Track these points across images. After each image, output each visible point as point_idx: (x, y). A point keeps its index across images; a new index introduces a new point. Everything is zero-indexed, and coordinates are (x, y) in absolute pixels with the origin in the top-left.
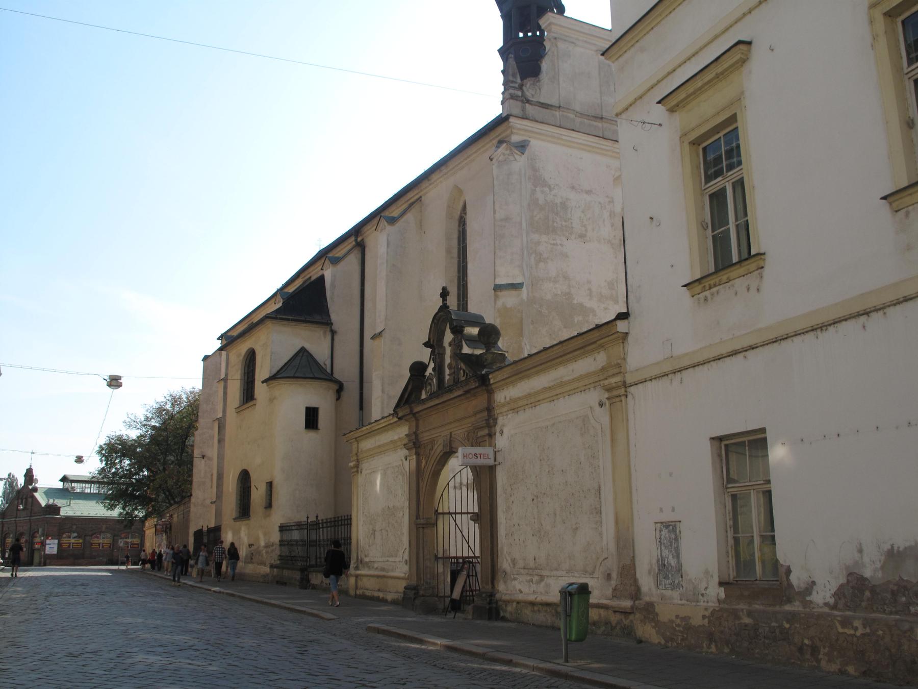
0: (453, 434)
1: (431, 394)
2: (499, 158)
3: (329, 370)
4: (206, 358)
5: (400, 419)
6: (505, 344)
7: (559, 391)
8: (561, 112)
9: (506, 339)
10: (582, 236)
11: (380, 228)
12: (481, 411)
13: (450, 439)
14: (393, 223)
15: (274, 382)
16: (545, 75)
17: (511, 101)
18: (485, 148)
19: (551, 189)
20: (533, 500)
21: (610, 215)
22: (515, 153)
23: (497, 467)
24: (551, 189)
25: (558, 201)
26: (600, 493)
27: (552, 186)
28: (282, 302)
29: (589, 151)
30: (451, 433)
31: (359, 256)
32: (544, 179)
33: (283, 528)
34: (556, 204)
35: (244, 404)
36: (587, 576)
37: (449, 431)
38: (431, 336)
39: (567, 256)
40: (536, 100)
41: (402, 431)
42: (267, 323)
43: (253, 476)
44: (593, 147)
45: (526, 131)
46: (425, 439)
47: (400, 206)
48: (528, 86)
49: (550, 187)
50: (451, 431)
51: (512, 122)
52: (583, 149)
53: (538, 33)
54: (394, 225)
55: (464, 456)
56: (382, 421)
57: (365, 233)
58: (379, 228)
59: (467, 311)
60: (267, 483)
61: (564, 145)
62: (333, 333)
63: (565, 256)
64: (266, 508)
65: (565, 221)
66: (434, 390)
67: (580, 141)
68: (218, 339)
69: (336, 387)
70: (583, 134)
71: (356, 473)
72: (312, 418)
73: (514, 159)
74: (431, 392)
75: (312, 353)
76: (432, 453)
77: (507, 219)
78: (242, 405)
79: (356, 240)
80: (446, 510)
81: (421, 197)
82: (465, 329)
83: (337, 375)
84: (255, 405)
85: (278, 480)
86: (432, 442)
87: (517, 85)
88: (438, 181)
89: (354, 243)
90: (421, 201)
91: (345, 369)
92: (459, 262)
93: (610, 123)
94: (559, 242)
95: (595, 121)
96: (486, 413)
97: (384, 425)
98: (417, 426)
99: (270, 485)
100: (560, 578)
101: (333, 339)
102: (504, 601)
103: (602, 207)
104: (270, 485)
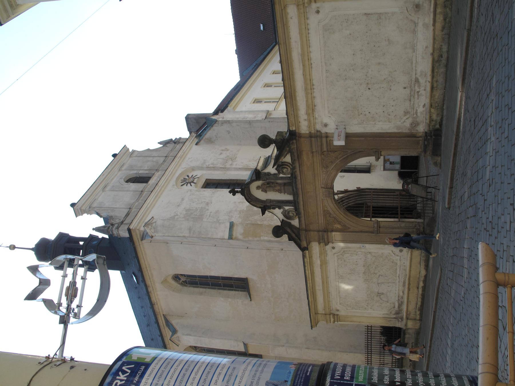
0: (323, 186)
2: (152, 232)
6: (265, 235)
7: (306, 58)
8: (133, 208)
9: (262, 234)
10: (207, 204)
11: (177, 342)
13: (325, 188)
14: (176, 331)
16: (109, 214)
17: (120, 229)
18: (144, 254)
21: (198, 191)
23: (348, 132)
25: (184, 212)
26: (369, 14)
27: (175, 214)
32: (170, 217)
34: (186, 213)
36: (416, 30)
39: (218, 211)
41: (315, 247)
44: (157, 195)
45: (139, 223)
47: (166, 334)
48: (113, 221)
50: (320, 187)
51: (133, 228)
53: (81, 243)
55: (339, 140)
58: (177, 342)
61: (152, 208)
63: (217, 212)
65: (197, 210)
66: (293, 209)
67: (152, 200)
70: (149, 198)
71: (338, 316)
73: (155, 223)
74: (294, 211)
77: (190, 229)
82: (258, 169)
86: (326, 213)
87: (111, 227)
88: (157, 298)
92: (209, 288)
93: (146, 188)
94: (209, 214)
95: (143, 195)
96: (313, 139)
97: (310, 272)
100: (417, 61)
102: (430, 122)
103: (192, 195)
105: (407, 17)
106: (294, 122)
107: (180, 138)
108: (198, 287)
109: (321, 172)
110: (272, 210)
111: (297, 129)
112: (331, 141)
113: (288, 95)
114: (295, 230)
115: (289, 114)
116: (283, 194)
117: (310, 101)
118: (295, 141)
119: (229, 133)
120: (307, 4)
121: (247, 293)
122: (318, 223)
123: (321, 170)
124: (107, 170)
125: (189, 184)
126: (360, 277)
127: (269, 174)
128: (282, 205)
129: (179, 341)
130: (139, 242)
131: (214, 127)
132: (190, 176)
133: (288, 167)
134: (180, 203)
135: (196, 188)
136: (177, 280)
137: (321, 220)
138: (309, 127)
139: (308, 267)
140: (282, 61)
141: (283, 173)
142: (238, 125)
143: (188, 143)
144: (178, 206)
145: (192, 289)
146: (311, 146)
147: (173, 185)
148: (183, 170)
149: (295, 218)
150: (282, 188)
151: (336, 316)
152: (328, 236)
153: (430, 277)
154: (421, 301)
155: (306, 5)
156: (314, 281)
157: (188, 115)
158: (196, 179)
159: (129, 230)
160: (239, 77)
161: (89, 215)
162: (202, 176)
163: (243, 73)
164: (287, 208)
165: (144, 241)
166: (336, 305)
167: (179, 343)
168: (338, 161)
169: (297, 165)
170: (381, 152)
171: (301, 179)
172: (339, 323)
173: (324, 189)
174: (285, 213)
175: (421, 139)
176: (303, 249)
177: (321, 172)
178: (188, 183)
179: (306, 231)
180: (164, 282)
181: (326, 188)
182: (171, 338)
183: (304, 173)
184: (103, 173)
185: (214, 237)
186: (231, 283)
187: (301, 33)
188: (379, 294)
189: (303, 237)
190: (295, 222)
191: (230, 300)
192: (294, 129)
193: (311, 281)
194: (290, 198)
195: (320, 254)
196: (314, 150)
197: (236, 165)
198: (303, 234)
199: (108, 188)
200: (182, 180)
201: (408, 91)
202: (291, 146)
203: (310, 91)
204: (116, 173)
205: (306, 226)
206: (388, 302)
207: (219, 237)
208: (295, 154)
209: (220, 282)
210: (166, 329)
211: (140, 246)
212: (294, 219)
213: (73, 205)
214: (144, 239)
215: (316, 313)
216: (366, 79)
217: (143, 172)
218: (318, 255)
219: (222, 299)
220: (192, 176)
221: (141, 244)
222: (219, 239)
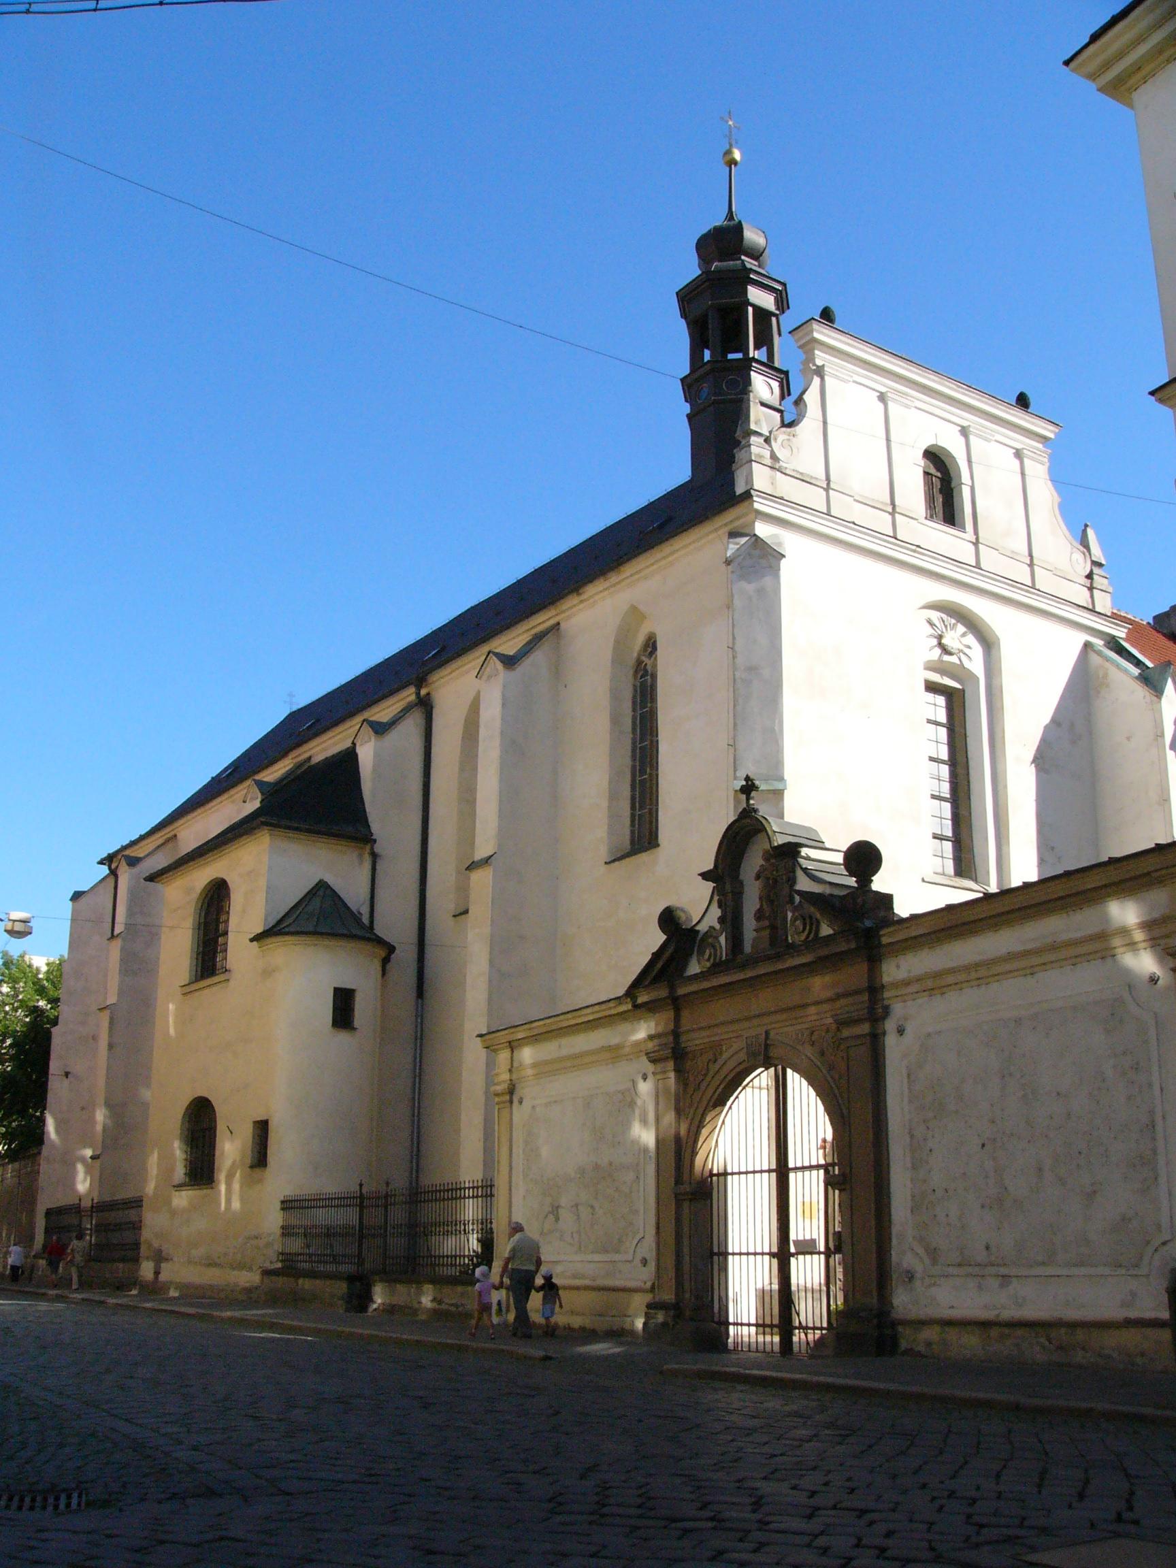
0: (772, 1034)
1: (714, 965)
3: (365, 920)
5: (636, 1006)
12: (857, 992)
15: (273, 942)
20: (983, 1145)
28: (259, 800)
30: (767, 1033)
33: (288, 1205)
35: (196, 981)
37: (764, 1028)
38: (720, 861)
40: (792, 468)
41: (681, 1030)
42: (257, 836)
46: (697, 1042)
54: (514, 670)
57: (434, 682)
58: (488, 670)
59: (782, 817)
60: (256, 1123)
62: (375, 856)
66: (721, 958)
68: (101, 862)
69: (383, 954)
74: (715, 959)
76: (714, 1068)
78: (193, 983)
79: (418, 694)
83: (379, 930)
86: (716, 1049)
89: (413, 697)
90: (558, 629)
96: (865, 997)
97: (591, 1018)
98: (677, 1019)
99: (262, 1128)
101: (374, 869)
104: (262, 1128)
117: (950, 979)
129: (489, 677)
130: (726, 525)
133: (806, 933)
136: (648, 646)
138: (896, 985)
141: (794, 919)
145: (628, 694)
153: (13, 1236)
155: (1162, 942)
164: (722, 939)
167: (485, 677)
174: (711, 936)
176: (631, 992)
177: (799, 1027)
194: (748, 948)
201: (981, 1256)
203: (973, 975)
206: (541, 1234)
209: (648, 770)
210: (525, 635)
220: (969, 647)
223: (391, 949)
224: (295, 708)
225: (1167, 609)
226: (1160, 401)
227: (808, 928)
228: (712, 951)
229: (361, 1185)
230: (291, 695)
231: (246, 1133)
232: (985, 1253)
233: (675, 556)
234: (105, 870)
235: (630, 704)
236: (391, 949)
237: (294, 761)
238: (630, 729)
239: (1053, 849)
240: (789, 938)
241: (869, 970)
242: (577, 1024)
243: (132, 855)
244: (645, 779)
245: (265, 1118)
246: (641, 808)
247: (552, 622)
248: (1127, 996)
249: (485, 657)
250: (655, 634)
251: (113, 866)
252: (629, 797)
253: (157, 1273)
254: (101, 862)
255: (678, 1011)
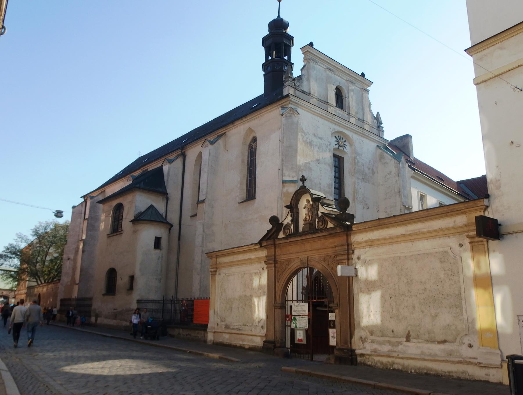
0: (309, 258)
4: (74, 207)
5: (261, 246)
11: (204, 146)
19: (305, 135)
20: (391, 297)
22: (295, 113)
24: (305, 135)
27: (306, 133)
28: (132, 181)
29: (322, 118)
31: (182, 160)
32: (303, 129)
35: (112, 233)
41: (263, 253)
43: (119, 272)
49: (305, 134)
52: (319, 117)
56: (245, 247)
58: (205, 145)
60: (129, 276)
62: (167, 199)
64: (128, 290)
66: (291, 233)
68: (81, 197)
69: (169, 227)
72: (158, 242)
74: (289, 233)
75: (157, 208)
79: (182, 152)
80: (289, 299)
81: (226, 132)
84: (122, 234)
85: (137, 274)
86: (289, 261)
88: (238, 125)
91: (173, 217)
92: (248, 167)
96: (346, 247)
97: (245, 249)
103: (326, 147)
105: (459, 334)
106: (359, 229)
107: (383, 131)
108: (248, 158)
109: (320, 256)
110: (290, 214)
111: (353, 232)
112: (345, 263)
113: (382, 222)
114: (275, 235)
115: (365, 223)
116: (303, 223)
118: (342, 230)
119: (389, 174)
120: (467, 234)
121: (245, 200)
122: (281, 255)
123: (321, 255)
124: (347, 70)
125: (337, 143)
126: (243, 292)
127: (317, 210)
128: (294, 222)
131: (393, 160)
132: (345, 143)
133: (323, 225)
134: (317, 136)
135: (334, 149)
137: (284, 258)
139: (247, 248)
140: (412, 214)
141: (318, 222)
142: (396, 182)
143: (378, 138)
144: (315, 135)
145: (246, 153)
146: (340, 246)
147: (335, 129)
148: (351, 136)
149: (284, 234)
150: (308, 222)
151: (215, 273)
152: (271, 264)
154: (227, 344)
156: (239, 254)
157: (411, 137)
158: (342, 149)
159: (288, 96)
160: (458, 181)
161: (303, 59)
162: (346, 153)
163: (463, 183)
164: (292, 227)
165: (280, 109)
166: (224, 271)
167: (204, 147)
168: (330, 271)
169: (324, 234)
170: (338, 309)
171: (314, 238)
172: (211, 276)
173: (307, 259)
175: (349, 346)
176: (260, 243)
177: (320, 256)
178: (338, 142)
179: (275, 244)
180: (250, 130)
181: (308, 261)
182: (208, 140)
183: (319, 241)
184: (344, 67)
185: (284, 168)
186: (252, 185)
187: (442, 230)
188: (231, 309)
189: (269, 242)
190: (281, 235)
191: (239, 186)
192: (354, 229)
193: (238, 251)
194: (301, 230)
195: (258, 257)
196: (337, 248)
197: (358, 183)
198: (270, 242)
199: (329, 73)
200: (341, 136)
202: (339, 227)
204: (345, 78)
205: (279, 244)
207: (284, 172)
208: (332, 232)
211: (276, 106)
212: (283, 234)
213: (311, 44)
214: (282, 109)
215: (217, 257)
216: (399, 294)
217: (345, 102)
218: (258, 256)
219: (239, 179)
220: (346, 145)
221: (278, 107)
222: (283, 172)
223: (172, 226)
224: (141, 156)
225: (395, 139)
226: (468, 53)
227: (324, 223)
228: (289, 231)
229: (163, 297)
230: (140, 152)
231: (126, 279)
232: (392, 333)
233: (230, 129)
234: (83, 200)
235: (247, 156)
236: (172, 226)
237: (143, 170)
238: (247, 165)
239: (367, 204)
240: (317, 227)
241: (347, 238)
242: (244, 250)
243: (92, 195)
244: (251, 179)
245: (133, 275)
246: (249, 187)
247: (224, 132)
248: (449, 251)
249: (204, 141)
250: (256, 137)
251: (85, 199)
252: (246, 184)
253: (96, 320)
254: (81, 197)
255: (275, 248)
